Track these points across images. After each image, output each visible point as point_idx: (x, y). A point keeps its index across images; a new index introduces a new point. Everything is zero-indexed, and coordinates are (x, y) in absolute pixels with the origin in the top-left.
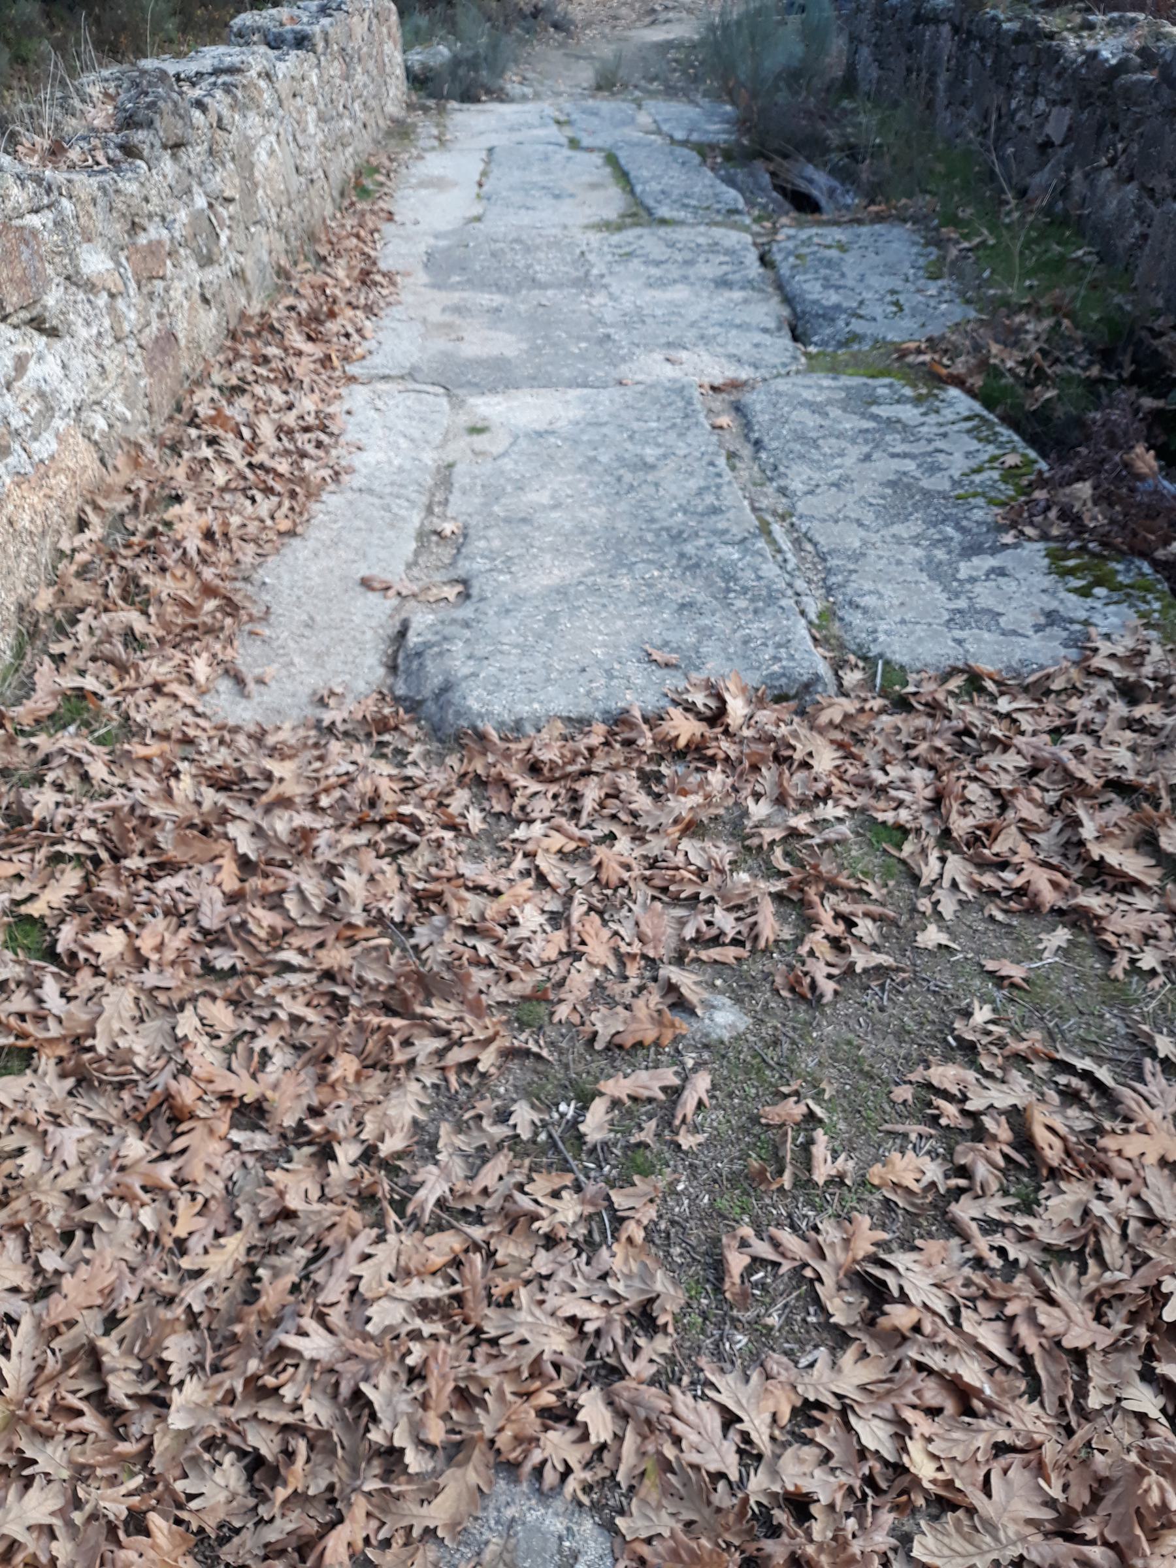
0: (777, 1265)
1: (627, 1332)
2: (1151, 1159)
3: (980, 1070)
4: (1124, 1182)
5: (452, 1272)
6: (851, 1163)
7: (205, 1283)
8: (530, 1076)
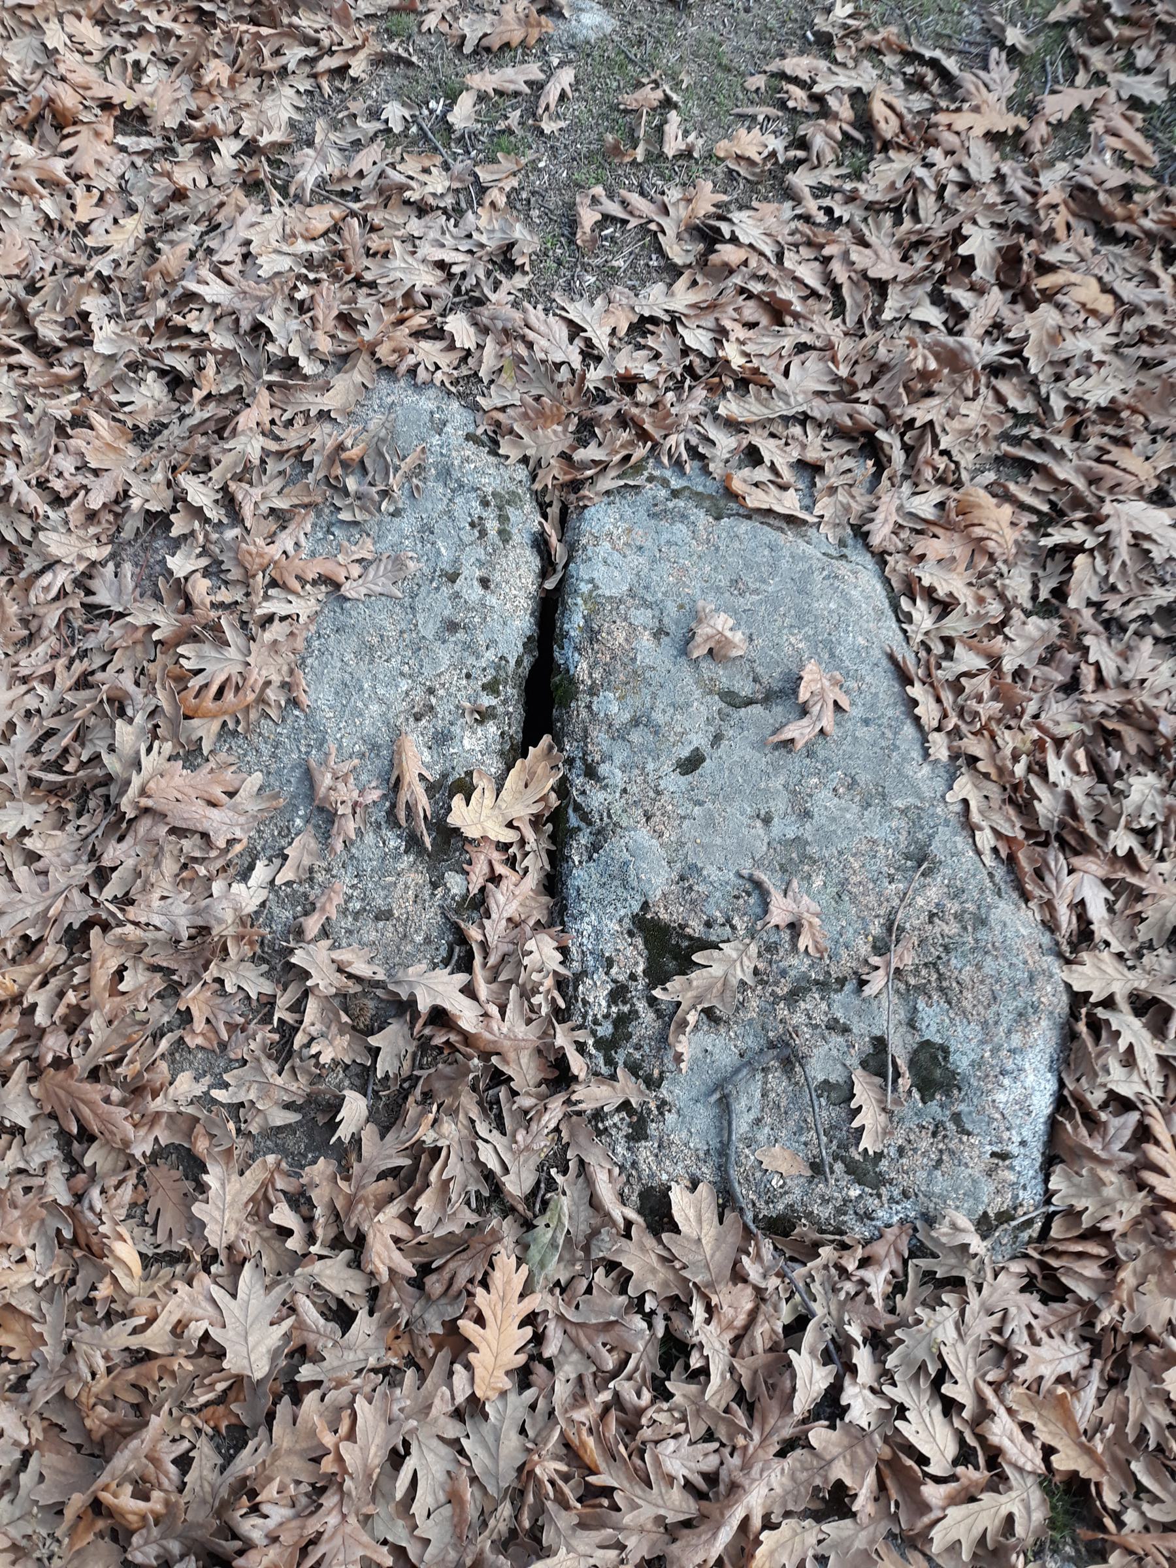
0: (625, 222)
1: (489, 273)
2: (979, 131)
3: (834, 61)
4: (950, 153)
5: (333, 236)
6: (701, 141)
7: (111, 256)
8: (400, 81)
